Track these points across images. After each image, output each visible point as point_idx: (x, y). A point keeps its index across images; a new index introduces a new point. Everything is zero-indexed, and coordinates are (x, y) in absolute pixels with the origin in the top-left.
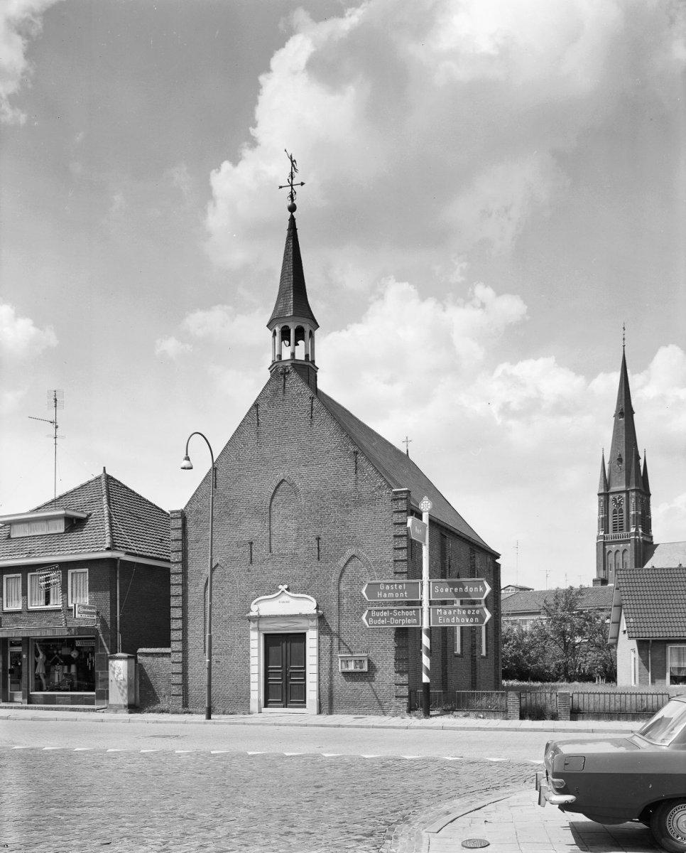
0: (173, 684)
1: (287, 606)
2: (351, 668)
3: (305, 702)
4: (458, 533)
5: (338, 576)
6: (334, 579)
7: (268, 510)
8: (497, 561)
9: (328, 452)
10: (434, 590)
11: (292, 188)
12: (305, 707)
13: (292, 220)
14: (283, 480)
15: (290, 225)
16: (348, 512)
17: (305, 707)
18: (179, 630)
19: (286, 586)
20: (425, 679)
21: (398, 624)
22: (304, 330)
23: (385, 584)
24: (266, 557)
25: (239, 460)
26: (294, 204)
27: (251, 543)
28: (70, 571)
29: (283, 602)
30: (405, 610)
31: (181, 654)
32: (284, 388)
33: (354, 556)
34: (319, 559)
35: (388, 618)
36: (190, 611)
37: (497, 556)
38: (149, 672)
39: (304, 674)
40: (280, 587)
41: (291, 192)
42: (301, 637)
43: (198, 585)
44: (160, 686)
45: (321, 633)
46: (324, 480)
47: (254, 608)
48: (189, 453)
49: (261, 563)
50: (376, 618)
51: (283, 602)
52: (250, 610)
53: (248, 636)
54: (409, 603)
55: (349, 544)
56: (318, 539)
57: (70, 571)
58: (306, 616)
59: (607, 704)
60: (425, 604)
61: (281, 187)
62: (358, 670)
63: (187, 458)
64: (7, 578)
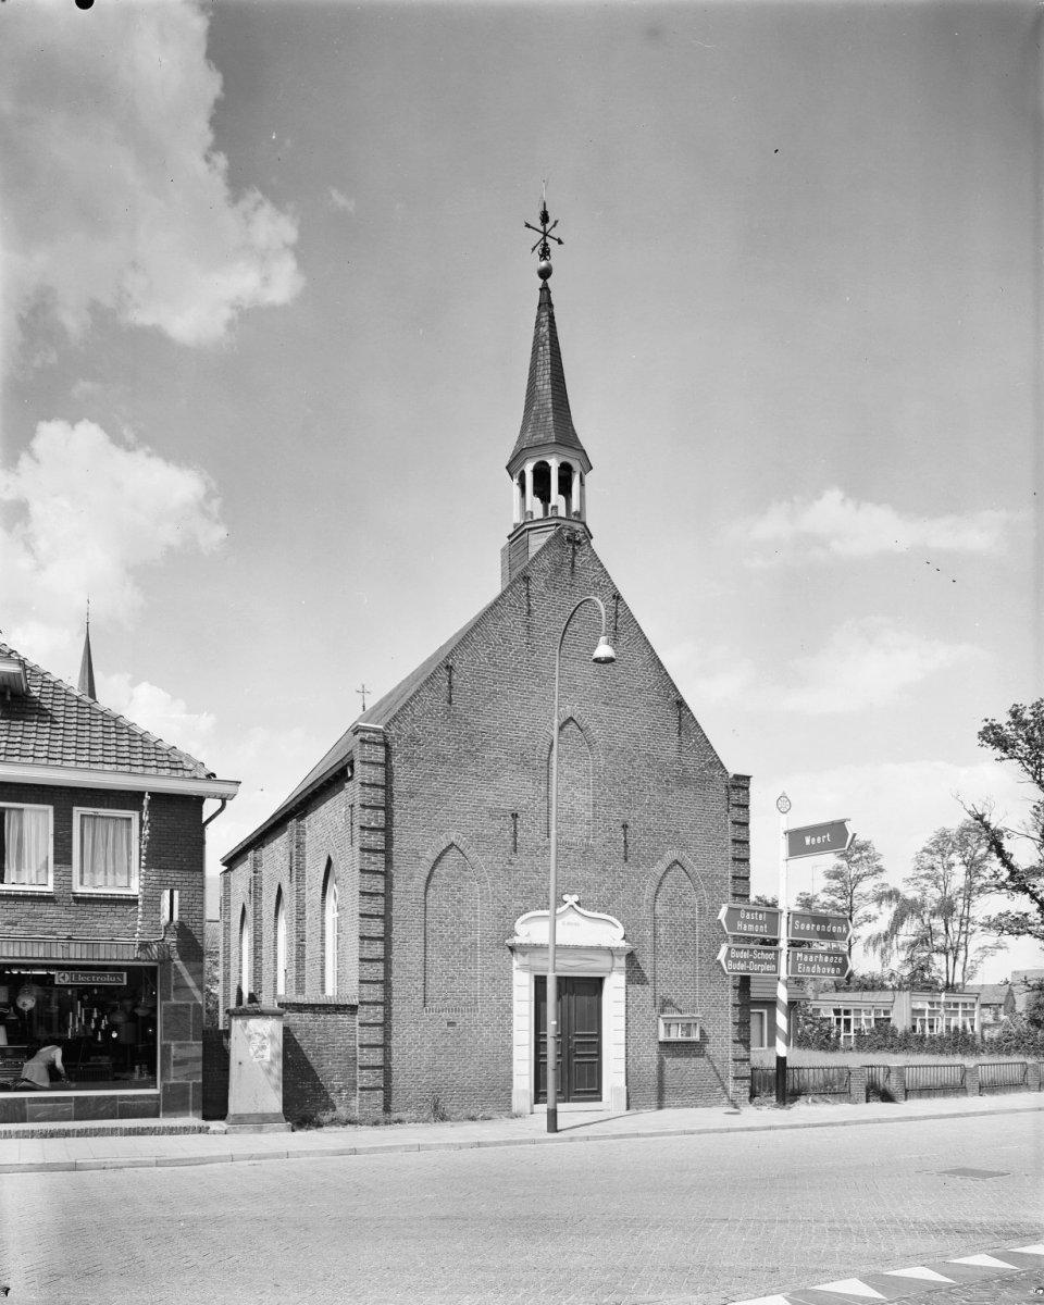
0: (362, 1068)
1: (583, 932)
2: (677, 1035)
3: (599, 1092)
5: (653, 890)
6: (649, 891)
7: (545, 764)
9: (640, 690)
10: (794, 925)
12: (600, 1100)
13: (545, 289)
14: (571, 719)
16: (668, 792)
17: (600, 1100)
18: (378, 960)
19: (576, 898)
21: (744, 971)
23: (747, 911)
24: (541, 844)
25: (495, 665)
26: (550, 265)
27: (515, 816)
28: (77, 811)
29: (568, 924)
30: (765, 951)
31: (380, 1009)
32: (573, 566)
33: (676, 862)
35: (747, 961)
36: (396, 927)
38: (304, 1044)
39: (599, 1046)
40: (566, 897)
42: (595, 985)
43: (411, 877)
44: (330, 1071)
45: (629, 981)
46: (635, 735)
47: (519, 927)
49: (532, 852)
50: (735, 960)
51: (568, 924)
52: (512, 933)
53: (509, 979)
54: (764, 942)
55: (668, 843)
56: (625, 827)
57: (77, 811)
58: (611, 951)
59: (796, 1084)
60: (783, 944)
61: (528, 226)
62: (685, 1039)
64: (82, 816)
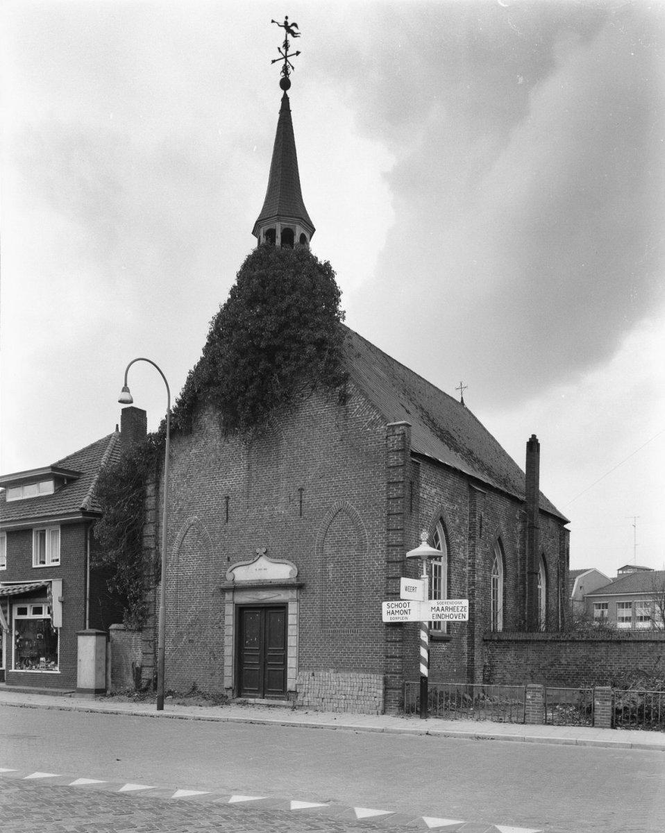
4: (263, 606)
8: (566, 526)
11: (286, 61)
13: (285, 100)
15: (281, 112)
20: (424, 670)
22: (287, 229)
34: (301, 515)
37: (566, 522)
41: (285, 65)
42: (282, 607)
48: (128, 384)
61: (274, 61)
63: (126, 389)
